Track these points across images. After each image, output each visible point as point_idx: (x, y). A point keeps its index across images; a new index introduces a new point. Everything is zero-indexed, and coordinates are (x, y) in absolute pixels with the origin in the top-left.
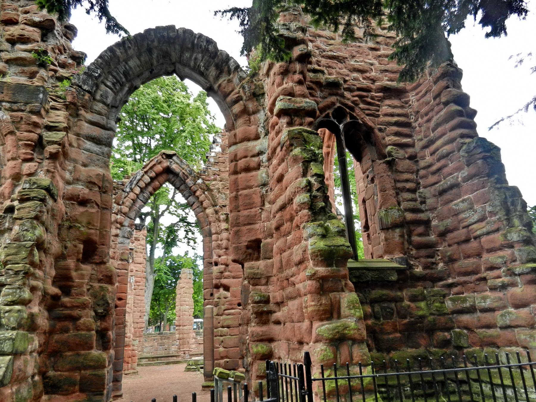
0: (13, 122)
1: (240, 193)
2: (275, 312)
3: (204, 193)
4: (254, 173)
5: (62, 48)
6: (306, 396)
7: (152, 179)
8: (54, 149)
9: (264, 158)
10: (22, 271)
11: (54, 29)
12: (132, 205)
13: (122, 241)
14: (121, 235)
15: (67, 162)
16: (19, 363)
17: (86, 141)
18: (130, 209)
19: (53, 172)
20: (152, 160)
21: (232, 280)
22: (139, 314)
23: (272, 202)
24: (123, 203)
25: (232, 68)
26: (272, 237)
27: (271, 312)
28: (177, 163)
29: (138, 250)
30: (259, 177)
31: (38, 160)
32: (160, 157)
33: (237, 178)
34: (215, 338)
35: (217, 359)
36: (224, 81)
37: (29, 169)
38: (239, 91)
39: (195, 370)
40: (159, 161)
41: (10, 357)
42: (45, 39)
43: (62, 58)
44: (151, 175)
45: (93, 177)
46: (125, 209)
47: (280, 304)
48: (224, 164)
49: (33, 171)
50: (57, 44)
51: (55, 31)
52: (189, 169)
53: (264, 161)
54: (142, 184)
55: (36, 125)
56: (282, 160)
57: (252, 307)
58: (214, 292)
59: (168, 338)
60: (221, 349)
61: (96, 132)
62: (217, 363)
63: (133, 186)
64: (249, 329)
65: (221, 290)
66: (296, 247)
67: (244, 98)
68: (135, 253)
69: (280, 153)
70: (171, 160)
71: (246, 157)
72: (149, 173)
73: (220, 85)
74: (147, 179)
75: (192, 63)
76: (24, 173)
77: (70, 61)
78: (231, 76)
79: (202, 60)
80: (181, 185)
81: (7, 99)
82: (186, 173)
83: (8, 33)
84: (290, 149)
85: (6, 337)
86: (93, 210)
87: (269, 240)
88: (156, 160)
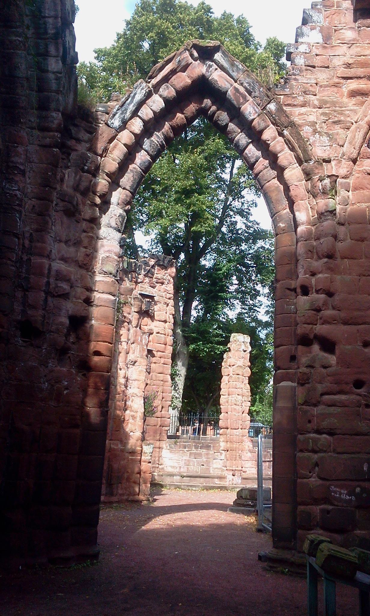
40: (183, 63)
58: (299, 353)
88: (178, 60)
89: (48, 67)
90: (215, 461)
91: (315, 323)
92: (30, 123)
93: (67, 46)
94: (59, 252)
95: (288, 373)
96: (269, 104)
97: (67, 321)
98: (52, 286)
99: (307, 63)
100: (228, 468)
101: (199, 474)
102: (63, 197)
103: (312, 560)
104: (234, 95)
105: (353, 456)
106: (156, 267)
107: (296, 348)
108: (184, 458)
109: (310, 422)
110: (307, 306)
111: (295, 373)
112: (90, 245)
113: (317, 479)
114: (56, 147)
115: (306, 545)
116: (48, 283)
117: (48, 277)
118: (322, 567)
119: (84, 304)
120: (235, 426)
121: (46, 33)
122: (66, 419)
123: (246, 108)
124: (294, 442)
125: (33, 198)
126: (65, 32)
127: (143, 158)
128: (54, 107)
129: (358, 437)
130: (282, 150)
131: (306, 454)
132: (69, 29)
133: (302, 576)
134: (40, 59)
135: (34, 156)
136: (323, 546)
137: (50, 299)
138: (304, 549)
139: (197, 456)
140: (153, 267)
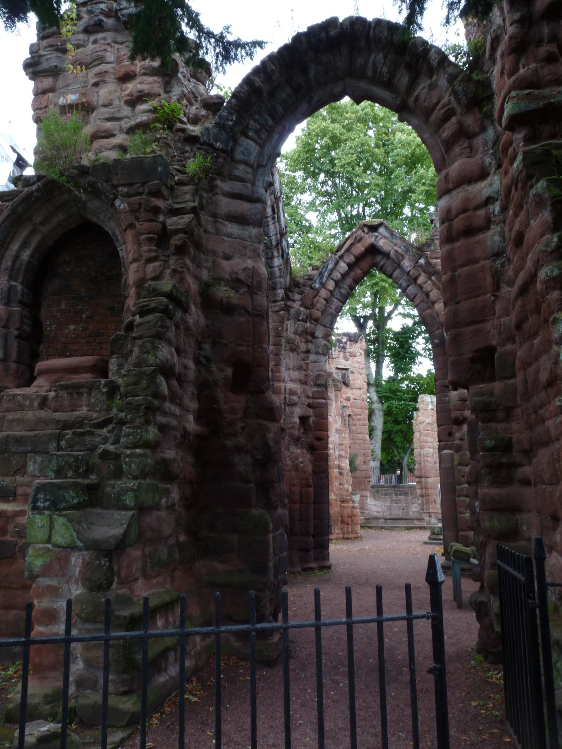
0: (132, 211)
1: (457, 273)
2: (521, 465)
4: (481, 236)
5: (191, 96)
6: (538, 611)
7: (351, 266)
8: (179, 240)
9: (496, 208)
10: (142, 405)
11: (178, 71)
12: (326, 306)
13: (316, 359)
14: (313, 350)
15: (202, 256)
16: (150, 519)
17: (226, 223)
18: (323, 313)
19: (181, 272)
23: (510, 283)
25: (435, 64)
26: (514, 342)
27: (513, 466)
28: (385, 237)
29: (355, 370)
30: (489, 243)
31: (163, 258)
33: (453, 249)
36: (423, 88)
37: (154, 270)
38: (449, 100)
40: (358, 238)
41: (133, 512)
42: (168, 89)
43: (193, 110)
44: (348, 260)
45: (239, 272)
47: (529, 453)
49: (157, 273)
50: (183, 91)
51: (180, 75)
52: (404, 244)
53: (496, 213)
54: (337, 275)
55: (156, 210)
56: (520, 207)
57: (482, 456)
61: (243, 207)
63: (324, 279)
64: (479, 490)
66: (544, 358)
67: (459, 110)
68: (350, 375)
69: (516, 196)
70: (376, 234)
71: (465, 211)
72: (345, 258)
73: (417, 98)
74: (343, 266)
75: (370, 72)
76: (148, 278)
77: (203, 112)
78: (435, 77)
79: (385, 63)
80: (394, 270)
81: (122, 182)
82: (400, 251)
83: (127, 92)
84: (529, 184)
85: (128, 487)
86: (242, 319)
87: (509, 347)
88: (354, 237)
90: (413, 506)
94: (289, 376)
95: (447, 444)
97: (297, 420)
98: (288, 399)
100: (425, 511)
101: (401, 517)
102: (289, 341)
104: (395, 255)
106: (348, 343)
107: (452, 428)
108: (387, 504)
109: (463, 477)
110: (457, 399)
112: (308, 368)
114: (282, 310)
116: (285, 398)
117: (285, 394)
123: (404, 263)
124: (454, 490)
130: (432, 290)
131: (462, 498)
134: (269, 261)
137: (287, 408)
139: (397, 501)
140: (346, 343)
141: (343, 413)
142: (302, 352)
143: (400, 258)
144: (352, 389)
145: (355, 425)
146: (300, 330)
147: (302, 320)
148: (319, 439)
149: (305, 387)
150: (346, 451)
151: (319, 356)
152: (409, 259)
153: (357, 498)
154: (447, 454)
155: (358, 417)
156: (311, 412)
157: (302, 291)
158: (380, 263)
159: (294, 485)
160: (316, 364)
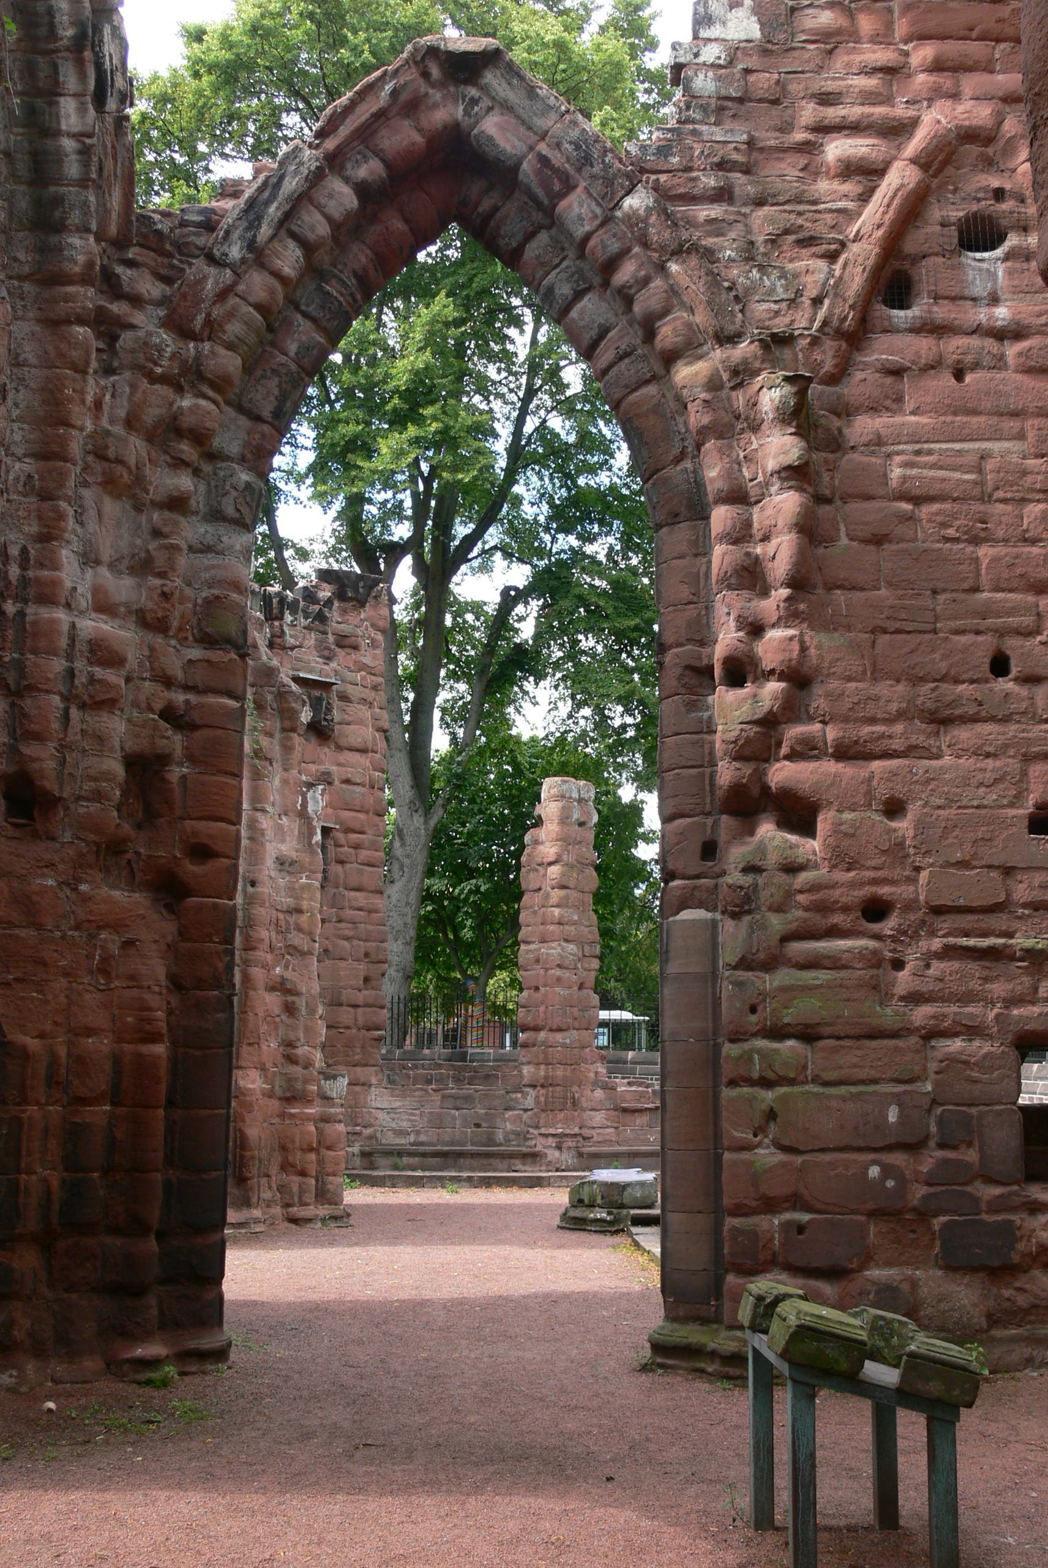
3: (662, 268)
13: (209, 539)
14: (198, 502)
18: (248, 369)
20: (370, 88)
21: (830, 767)
22: (362, 968)
24: (209, 322)
28: (507, 107)
29: (350, 690)
32: (412, 75)
34: (728, 1094)
35: (738, 1211)
39: (612, 1228)
40: (404, 97)
46: (229, 362)
48: (775, 111)
58: (723, 837)
59: (487, 1078)
60: (767, 1156)
62: (735, 1230)
63: (265, 231)
65: (767, 830)
68: (336, 703)
70: (473, 92)
80: (530, 236)
82: (557, 159)
88: (388, 87)
89: (59, 123)
91: (765, 756)
92: (16, 265)
93: (107, 65)
96: (627, 194)
97: (118, 768)
99: (723, 92)
103: (759, 1341)
104: (539, 173)
105: (860, 1088)
106: (336, 604)
107: (715, 823)
109: (753, 1010)
111: (716, 885)
113: (773, 1149)
115: (745, 1314)
116: (71, 673)
117: (70, 657)
118: (784, 1355)
119: (161, 722)
120: (557, 1021)
121: (53, 35)
122: (130, 1019)
125: (25, 455)
126: (101, 31)
127: (304, 338)
128: (77, 221)
129: (875, 1044)
132: (110, 21)
133: (739, 1380)
134: (39, 102)
135: (27, 349)
136: (782, 1308)
137: (74, 712)
138: (740, 1317)
139: (463, 1102)
140: (329, 603)
141: (305, 804)
142: (152, 502)
143: (557, 186)
144: (339, 748)
145: (341, 862)
146: (152, 414)
147: (164, 379)
148: (202, 852)
149: (159, 640)
150: (311, 934)
151: (222, 529)
152: (587, 190)
153: (340, 1086)
154: (693, 921)
155: (353, 837)
156: (175, 742)
157: (172, 266)
158: (477, 204)
159: (89, 1032)
160: (209, 560)
